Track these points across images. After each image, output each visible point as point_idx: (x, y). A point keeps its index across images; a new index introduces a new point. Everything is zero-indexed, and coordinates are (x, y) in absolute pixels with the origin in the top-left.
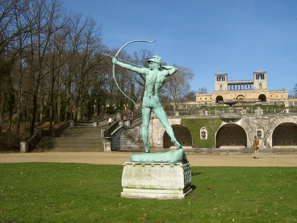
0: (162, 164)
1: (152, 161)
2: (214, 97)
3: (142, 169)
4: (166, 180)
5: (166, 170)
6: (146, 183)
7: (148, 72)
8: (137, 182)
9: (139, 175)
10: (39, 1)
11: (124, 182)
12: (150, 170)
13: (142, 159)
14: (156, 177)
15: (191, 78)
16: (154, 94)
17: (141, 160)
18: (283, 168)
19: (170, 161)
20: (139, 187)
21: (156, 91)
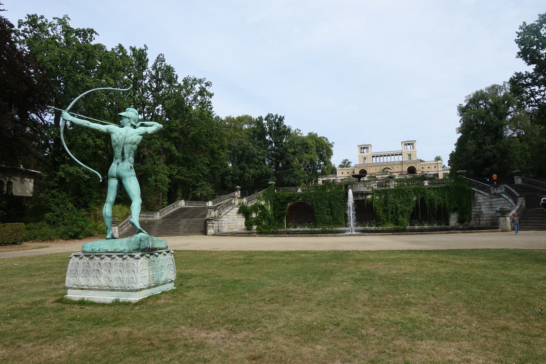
0: (114, 255)
2: (405, 169)
5: (118, 263)
6: (93, 282)
7: (112, 130)
8: (83, 281)
9: (87, 273)
11: (69, 280)
13: (93, 248)
15: (349, 163)
16: (123, 160)
17: (92, 250)
18: (315, 252)
19: (124, 250)
20: (86, 287)
21: (126, 155)
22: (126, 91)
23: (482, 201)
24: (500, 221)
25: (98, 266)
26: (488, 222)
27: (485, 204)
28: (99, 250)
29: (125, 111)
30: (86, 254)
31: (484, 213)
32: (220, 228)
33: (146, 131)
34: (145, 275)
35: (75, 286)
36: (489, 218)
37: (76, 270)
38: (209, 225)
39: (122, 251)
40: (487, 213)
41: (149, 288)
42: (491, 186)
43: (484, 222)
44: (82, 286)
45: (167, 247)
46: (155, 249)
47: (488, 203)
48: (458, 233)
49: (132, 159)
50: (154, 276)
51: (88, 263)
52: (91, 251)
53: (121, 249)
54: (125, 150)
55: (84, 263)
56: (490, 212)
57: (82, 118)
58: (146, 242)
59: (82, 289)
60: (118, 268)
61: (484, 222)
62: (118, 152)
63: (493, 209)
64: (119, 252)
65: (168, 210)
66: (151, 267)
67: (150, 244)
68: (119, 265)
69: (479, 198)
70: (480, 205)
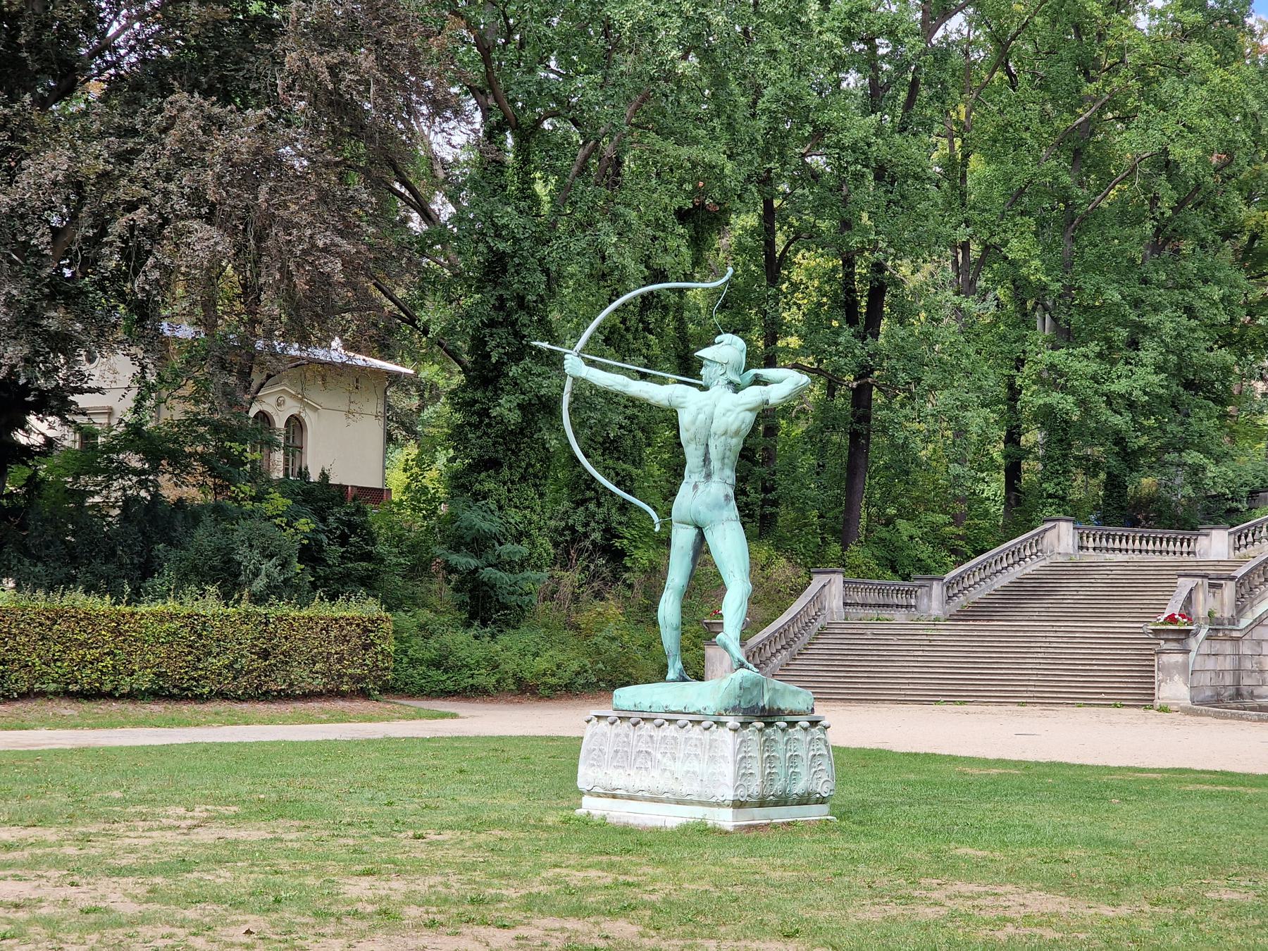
0: (683, 719)
1: (662, 710)
3: (631, 734)
4: (688, 772)
7: (680, 400)
8: (619, 779)
9: (622, 757)
10: (725, 1)
11: (587, 775)
12: (651, 737)
14: (665, 760)
16: (708, 476)
21: (715, 464)
22: (655, 509)
29: (714, 343)
30: (622, 714)
32: (1246, 681)
33: (765, 397)
34: (750, 771)
35: (597, 789)
38: (1165, 658)
41: (762, 803)
44: (614, 789)
45: (813, 709)
46: (779, 713)
49: (730, 475)
50: (773, 777)
51: (627, 736)
53: (699, 706)
54: (712, 450)
55: (617, 735)
57: (605, 368)
58: (755, 693)
59: (614, 797)
62: (693, 456)
64: (694, 713)
65: (988, 572)
66: (767, 754)
67: (766, 698)
68: (694, 742)
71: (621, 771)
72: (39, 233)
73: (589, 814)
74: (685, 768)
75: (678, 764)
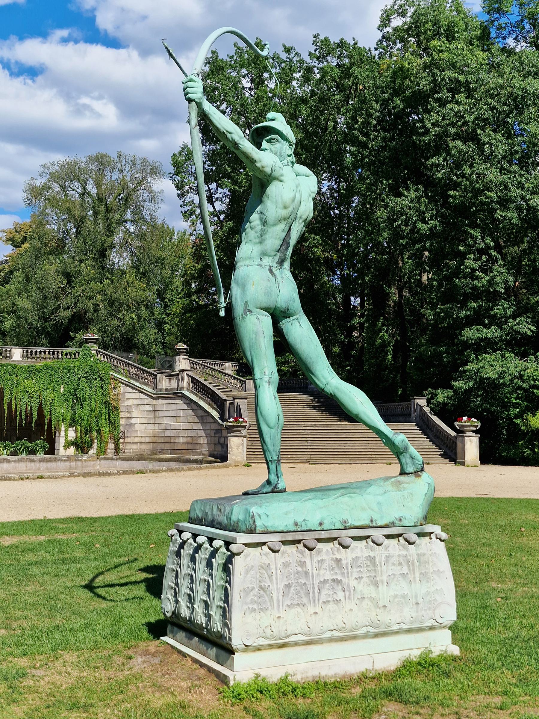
1: (338, 526)
4: (396, 596)
12: (338, 561)
17: (296, 524)
19: (400, 520)
23: (136, 402)
24: (232, 445)
25: (333, 569)
26: (143, 446)
27: (141, 408)
28: (321, 524)
31: (137, 427)
36: (147, 440)
37: (261, 588)
39: (393, 523)
40: (144, 427)
42: (158, 373)
43: (135, 447)
47: (149, 408)
48: (182, 470)
51: (303, 564)
52: (293, 528)
55: (286, 565)
56: (151, 427)
59: (283, 646)
60: (397, 570)
61: (135, 447)
63: (158, 420)
69: (127, 396)
70: (129, 412)
71: (299, 610)
72: (147, 681)
73: (258, 676)
74: (391, 593)
75: (383, 588)
